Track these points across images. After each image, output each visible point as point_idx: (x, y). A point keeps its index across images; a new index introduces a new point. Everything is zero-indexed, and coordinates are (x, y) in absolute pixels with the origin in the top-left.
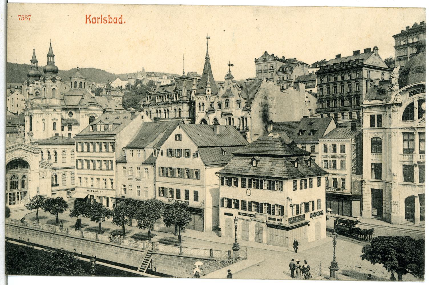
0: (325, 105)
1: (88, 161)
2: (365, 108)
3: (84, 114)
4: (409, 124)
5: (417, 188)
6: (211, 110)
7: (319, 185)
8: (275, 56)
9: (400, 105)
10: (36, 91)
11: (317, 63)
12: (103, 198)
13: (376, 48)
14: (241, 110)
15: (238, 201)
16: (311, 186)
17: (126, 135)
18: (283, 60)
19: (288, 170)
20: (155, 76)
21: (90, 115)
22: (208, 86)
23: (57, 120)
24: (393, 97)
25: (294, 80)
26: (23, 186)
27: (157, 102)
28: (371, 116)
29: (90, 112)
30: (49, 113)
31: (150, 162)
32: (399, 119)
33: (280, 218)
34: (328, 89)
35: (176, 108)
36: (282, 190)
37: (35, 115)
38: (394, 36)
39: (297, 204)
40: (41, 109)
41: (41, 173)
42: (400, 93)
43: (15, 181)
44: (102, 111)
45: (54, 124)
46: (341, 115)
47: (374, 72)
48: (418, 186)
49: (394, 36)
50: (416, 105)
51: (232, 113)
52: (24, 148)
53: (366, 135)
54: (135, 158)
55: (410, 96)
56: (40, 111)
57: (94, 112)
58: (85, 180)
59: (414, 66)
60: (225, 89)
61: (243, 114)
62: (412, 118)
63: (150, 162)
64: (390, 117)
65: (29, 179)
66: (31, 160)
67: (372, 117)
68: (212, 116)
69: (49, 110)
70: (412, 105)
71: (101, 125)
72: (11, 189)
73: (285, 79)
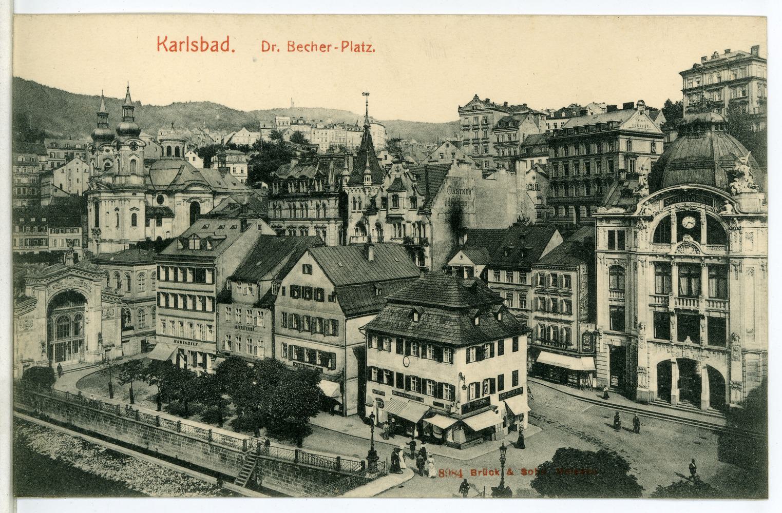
0: (562, 193)
1: (175, 296)
2: (601, 220)
3: (180, 199)
4: (663, 249)
5: (675, 349)
6: (372, 209)
7: (515, 349)
8: (491, 102)
9: (650, 219)
10: (106, 162)
11: (563, 109)
12: (198, 355)
13: (641, 103)
14: (416, 212)
15: (391, 373)
16: (501, 352)
17: (229, 262)
18: (505, 108)
19: (463, 330)
20: (304, 124)
21: (192, 201)
22: (368, 171)
23: (138, 210)
24: (639, 206)
25: (521, 141)
26: (77, 333)
27: (290, 192)
28: (609, 231)
29: (192, 195)
30: (125, 200)
31: (266, 302)
32: (648, 240)
33: (449, 403)
34: (567, 168)
35: (319, 202)
36: (452, 363)
37: (103, 202)
38: (681, 73)
39: (477, 381)
40: (114, 192)
41: (105, 311)
42: (649, 200)
43: (65, 326)
44: (211, 193)
45: (134, 217)
46: (585, 209)
47: (638, 142)
48: (677, 345)
49: (681, 73)
50: (674, 219)
51: (403, 216)
52: (79, 274)
53: (602, 261)
54: (244, 293)
55: (665, 206)
56: (112, 195)
57: (198, 195)
58: (171, 324)
59: (671, 159)
60: (393, 178)
61: (420, 218)
62: (668, 241)
63: (266, 302)
64: (635, 237)
65: (86, 321)
66: (88, 291)
67: (611, 234)
68: (372, 219)
69: (126, 194)
70: (668, 219)
71: (194, 239)
72: (58, 337)
73: (507, 139)
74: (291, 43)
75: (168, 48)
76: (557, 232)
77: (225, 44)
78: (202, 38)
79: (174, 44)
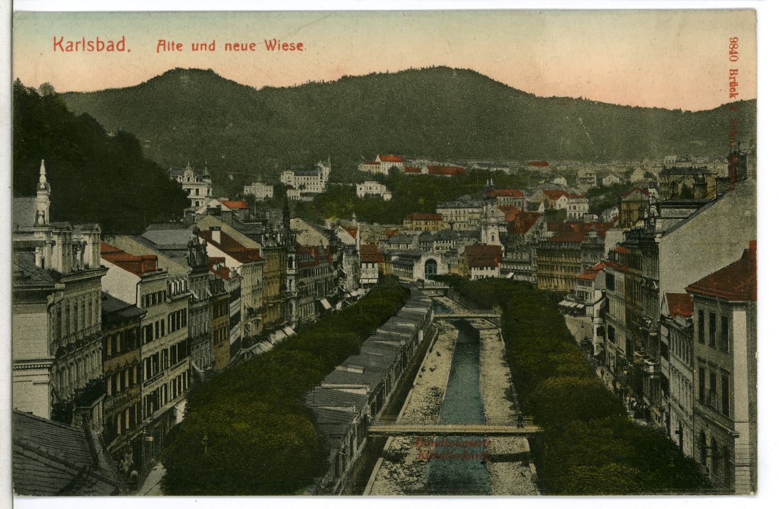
45: (493, 237)
74: (162, 43)
75: (64, 49)
76: (662, 326)
77: (121, 44)
78: (98, 38)
79: (70, 44)
